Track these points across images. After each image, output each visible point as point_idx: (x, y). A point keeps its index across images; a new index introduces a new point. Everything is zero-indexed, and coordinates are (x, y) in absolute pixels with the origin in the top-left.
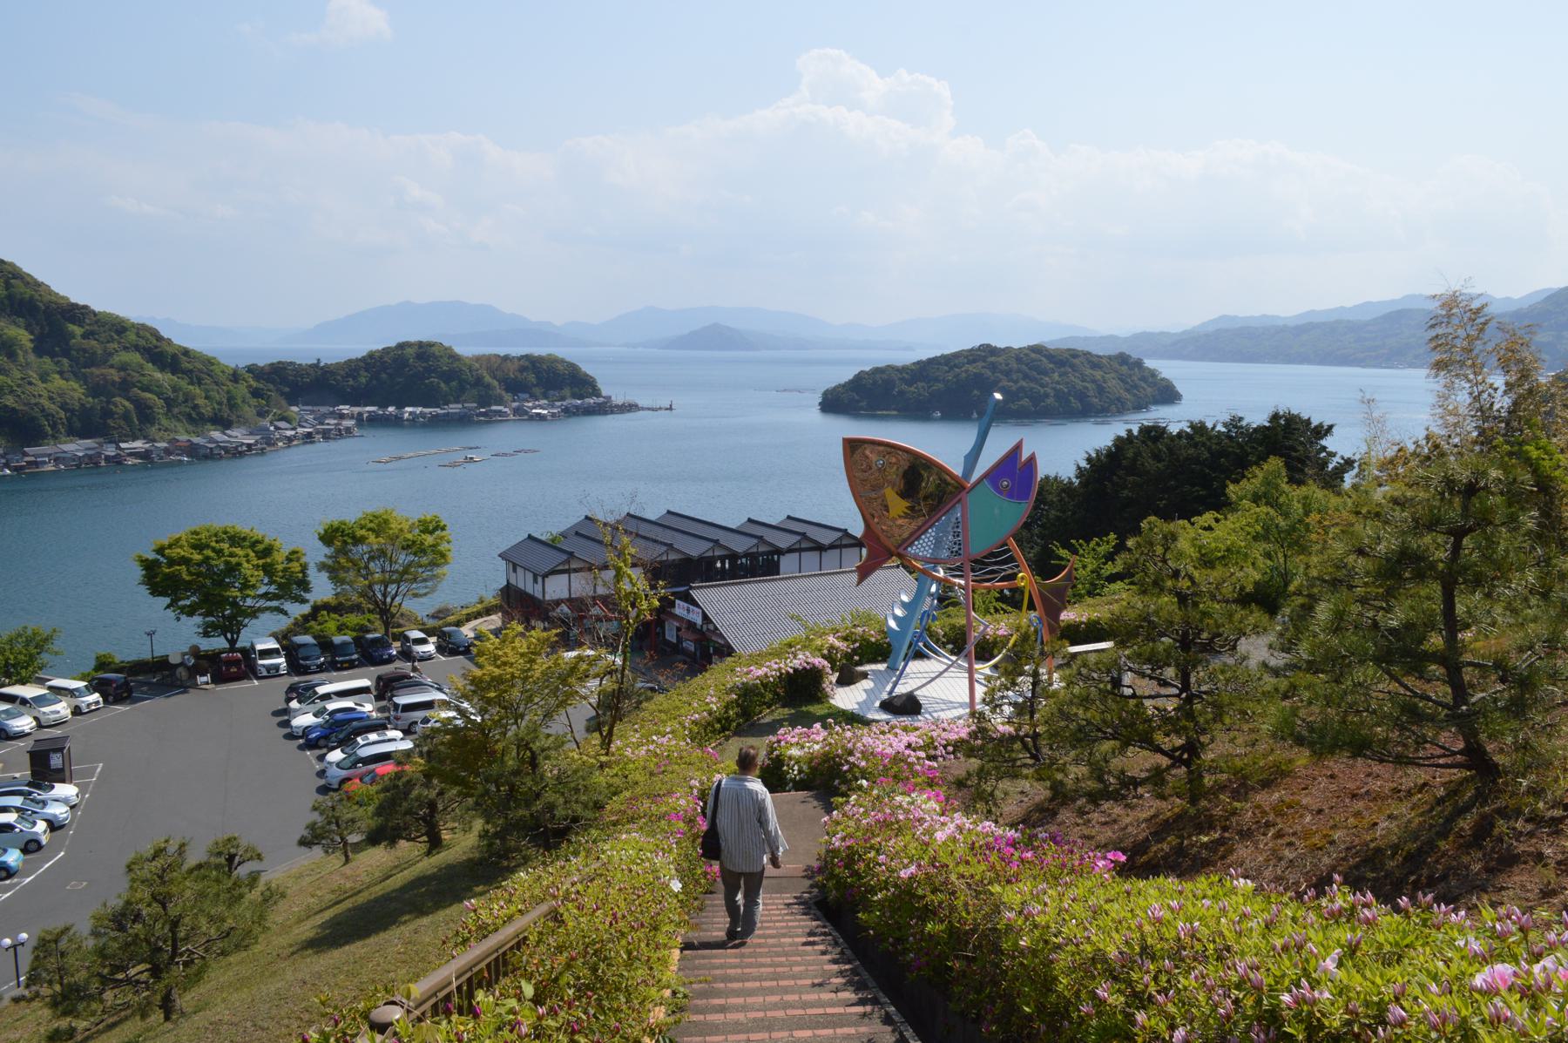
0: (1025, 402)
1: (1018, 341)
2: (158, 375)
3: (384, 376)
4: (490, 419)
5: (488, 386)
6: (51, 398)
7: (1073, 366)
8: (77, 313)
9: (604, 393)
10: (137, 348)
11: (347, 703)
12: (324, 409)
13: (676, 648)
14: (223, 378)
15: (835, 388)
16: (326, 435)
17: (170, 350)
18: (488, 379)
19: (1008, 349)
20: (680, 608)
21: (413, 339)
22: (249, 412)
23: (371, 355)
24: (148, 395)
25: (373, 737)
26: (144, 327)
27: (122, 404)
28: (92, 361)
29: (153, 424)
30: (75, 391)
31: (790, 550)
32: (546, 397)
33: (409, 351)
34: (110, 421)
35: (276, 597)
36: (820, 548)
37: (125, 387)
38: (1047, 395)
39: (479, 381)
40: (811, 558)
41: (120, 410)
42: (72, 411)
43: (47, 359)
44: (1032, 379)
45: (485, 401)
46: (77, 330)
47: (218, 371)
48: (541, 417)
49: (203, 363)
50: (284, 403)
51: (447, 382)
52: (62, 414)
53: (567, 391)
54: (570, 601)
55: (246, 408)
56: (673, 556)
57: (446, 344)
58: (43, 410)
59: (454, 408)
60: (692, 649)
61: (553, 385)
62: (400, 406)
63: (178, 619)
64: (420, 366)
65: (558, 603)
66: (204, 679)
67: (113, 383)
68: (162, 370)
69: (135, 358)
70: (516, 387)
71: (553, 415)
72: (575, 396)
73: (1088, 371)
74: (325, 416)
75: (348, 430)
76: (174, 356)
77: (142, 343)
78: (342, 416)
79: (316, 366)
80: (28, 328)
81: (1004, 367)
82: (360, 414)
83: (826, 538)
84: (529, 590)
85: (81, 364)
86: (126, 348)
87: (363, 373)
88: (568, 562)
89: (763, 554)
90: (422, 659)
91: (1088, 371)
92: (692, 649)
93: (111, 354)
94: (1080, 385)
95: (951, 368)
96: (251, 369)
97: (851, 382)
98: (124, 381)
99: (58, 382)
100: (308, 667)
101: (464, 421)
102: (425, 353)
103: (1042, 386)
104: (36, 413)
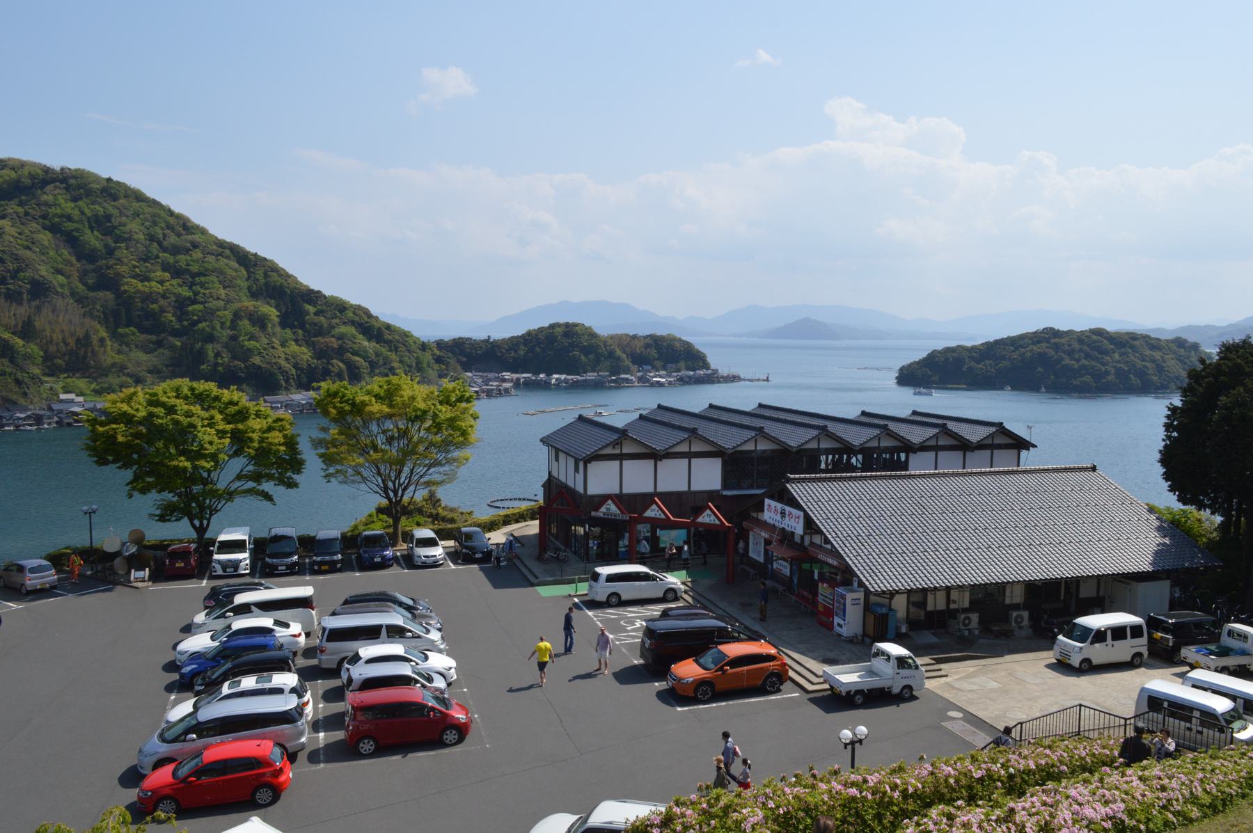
0: (1087, 378)
1: (1080, 326)
2: (366, 343)
3: (538, 349)
4: (619, 385)
5: (619, 359)
6: (287, 359)
7: (1132, 347)
8: (312, 296)
9: (712, 367)
10: (353, 323)
11: (266, 621)
12: (491, 375)
13: (764, 570)
14: (414, 347)
15: (910, 365)
16: (489, 394)
17: (377, 325)
18: (619, 352)
19: (1070, 332)
20: (772, 512)
21: (562, 320)
22: (432, 374)
23: (529, 333)
24: (357, 358)
25: (249, 682)
26: (359, 307)
28: (320, 332)
30: (304, 354)
31: (923, 448)
32: (664, 368)
33: (559, 329)
35: (257, 477)
36: (964, 446)
37: (340, 352)
38: (1107, 373)
39: (611, 354)
40: (950, 462)
41: (336, 370)
42: (302, 369)
43: (288, 331)
44: (1096, 359)
45: (615, 370)
47: (411, 342)
48: (660, 384)
49: (400, 335)
50: (459, 368)
51: (586, 355)
52: (294, 371)
53: (682, 364)
54: (620, 499)
55: (431, 371)
56: (763, 446)
57: (587, 325)
58: (280, 368)
59: (591, 376)
60: (787, 571)
61: (673, 356)
62: (549, 374)
63: (130, 496)
64: (566, 342)
65: (604, 499)
66: (141, 574)
67: (333, 349)
68: (369, 340)
69: (350, 330)
70: (640, 360)
71: (670, 383)
72: (688, 369)
73: (1148, 352)
74: (490, 380)
75: (506, 390)
77: (357, 319)
78: (504, 380)
79: (487, 341)
80: (277, 307)
81: (1066, 347)
82: (518, 379)
83: (974, 435)
84: (570, 483)
85: (310, 333)
86: (345, 323)
87: (522, 347)
88: (615, 444)
89: (886, 450)
90: (425, 566)
91: (1148, 352)
92: (787, 571)
93: (333, 327)
94: (1139, 364)
95: (1016, 349)
96: (440, 344)
97: (925, 359)
98: (341, 347)
99: (294, 347)
100: (275, 567)
101: (598, 386)
102: (571, 332)
103: (1103, 364)
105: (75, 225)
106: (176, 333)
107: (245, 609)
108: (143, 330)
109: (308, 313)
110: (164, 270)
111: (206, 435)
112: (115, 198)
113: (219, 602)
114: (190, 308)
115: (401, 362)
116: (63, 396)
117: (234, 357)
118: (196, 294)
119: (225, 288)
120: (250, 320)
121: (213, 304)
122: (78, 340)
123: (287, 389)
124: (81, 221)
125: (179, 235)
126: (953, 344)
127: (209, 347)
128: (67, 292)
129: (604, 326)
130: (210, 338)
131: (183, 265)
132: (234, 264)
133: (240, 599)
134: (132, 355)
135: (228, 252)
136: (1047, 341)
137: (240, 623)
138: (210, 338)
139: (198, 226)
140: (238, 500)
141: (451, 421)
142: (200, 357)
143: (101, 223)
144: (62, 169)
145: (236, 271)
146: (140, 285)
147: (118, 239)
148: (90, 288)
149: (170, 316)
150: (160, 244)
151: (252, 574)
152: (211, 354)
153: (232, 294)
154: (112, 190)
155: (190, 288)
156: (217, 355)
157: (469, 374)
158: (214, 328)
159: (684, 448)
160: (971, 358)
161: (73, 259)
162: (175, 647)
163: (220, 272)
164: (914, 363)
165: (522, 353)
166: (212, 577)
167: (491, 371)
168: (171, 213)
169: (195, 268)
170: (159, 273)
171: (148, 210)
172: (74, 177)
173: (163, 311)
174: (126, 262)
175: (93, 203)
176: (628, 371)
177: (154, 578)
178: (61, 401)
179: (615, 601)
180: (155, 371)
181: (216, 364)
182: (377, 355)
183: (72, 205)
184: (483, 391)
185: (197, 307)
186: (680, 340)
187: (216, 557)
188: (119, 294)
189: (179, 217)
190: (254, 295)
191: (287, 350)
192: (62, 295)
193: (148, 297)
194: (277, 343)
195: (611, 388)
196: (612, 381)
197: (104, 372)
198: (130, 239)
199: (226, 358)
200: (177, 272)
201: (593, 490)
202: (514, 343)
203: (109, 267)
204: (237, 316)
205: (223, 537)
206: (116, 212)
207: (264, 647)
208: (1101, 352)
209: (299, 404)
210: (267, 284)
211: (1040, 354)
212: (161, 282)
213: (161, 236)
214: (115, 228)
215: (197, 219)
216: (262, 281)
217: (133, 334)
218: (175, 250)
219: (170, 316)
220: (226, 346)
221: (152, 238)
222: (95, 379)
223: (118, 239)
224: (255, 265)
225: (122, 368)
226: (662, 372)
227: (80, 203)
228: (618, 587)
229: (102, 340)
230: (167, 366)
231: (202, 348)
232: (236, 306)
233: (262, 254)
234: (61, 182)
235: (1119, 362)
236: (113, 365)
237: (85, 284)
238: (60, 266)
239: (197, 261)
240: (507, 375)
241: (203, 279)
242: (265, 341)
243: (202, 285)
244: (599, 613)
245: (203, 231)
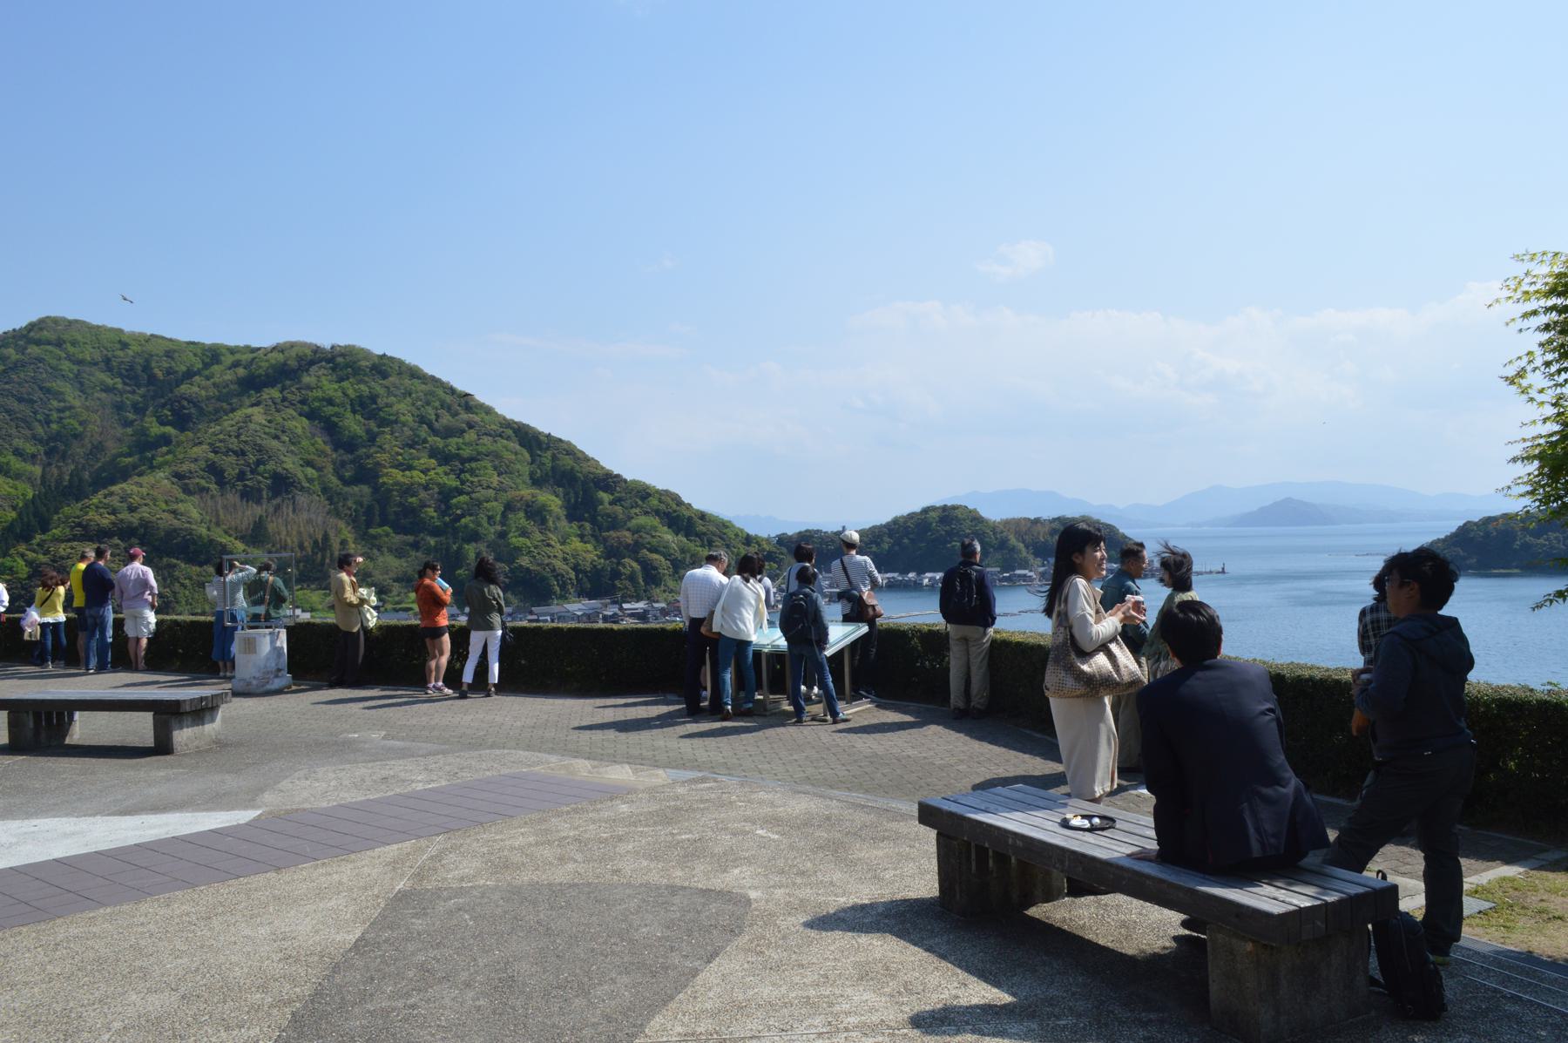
5: (1013, 549)
6: (565, 559)
8: (609, 481)
10: (657, 512)
18: (1013, 541)
23: (895, 521)
24: (655, 556)
26: (667, 492)
27: (630, 565)
28: (615, 524)
29: (658, 585)
30: (589, 553)
33: (932, 514)
34: (617, 583)
37: (634, 549)
39: (1003, 544)
42: (585, 572)
46: (605, 497)
49: (717, 526)
52: (572, 575)
58: (554, 570)
62: (921, 572)
64: (942, 530)
76: (690, 518)
77: (662, 507)
86: (646, 513)
87: (886, 539)
98: (636, 543)
99: (576, 544)
104: (547, 573)
105: (336, 409)
106: (435, 532)
108: (399, 529)
110: (431, 457)
121: (481, 494)
124: (342, 405)
128: (317, 487)
130: (474, 537)
135: (510, 432)
143: (366, 406)
147: (383, 423)
149: (431, 512)
150: (430, 426)
158: (479, 524)
161: (328, 449)
163: (497, 456)
165: (886, 546)
168: (452, 391)
169: (466, 453)
172: (343, 355)
176: (1025, 565)
182: (683, 551)
185: (463, 498)
190: (536, 482)
191: (567, 548)
193: (408, 490)
196: (1005, 579)
200: (444, 458)
203: (368, 457)
204: (509, 507)
212: (425, 472)
214: (380, 409)
215: (482, 396)
217: (387, 535)
218: (448, 433)
221: (422, 420)
223: (383, 423)
227: (345, 384)
231: (460, 548)
232: (511, 494)
233: (556, 434)
234: (329, 361)
237: (341, 478)
239: (469, 444)
241: (474, 465)
245: (489, 411)
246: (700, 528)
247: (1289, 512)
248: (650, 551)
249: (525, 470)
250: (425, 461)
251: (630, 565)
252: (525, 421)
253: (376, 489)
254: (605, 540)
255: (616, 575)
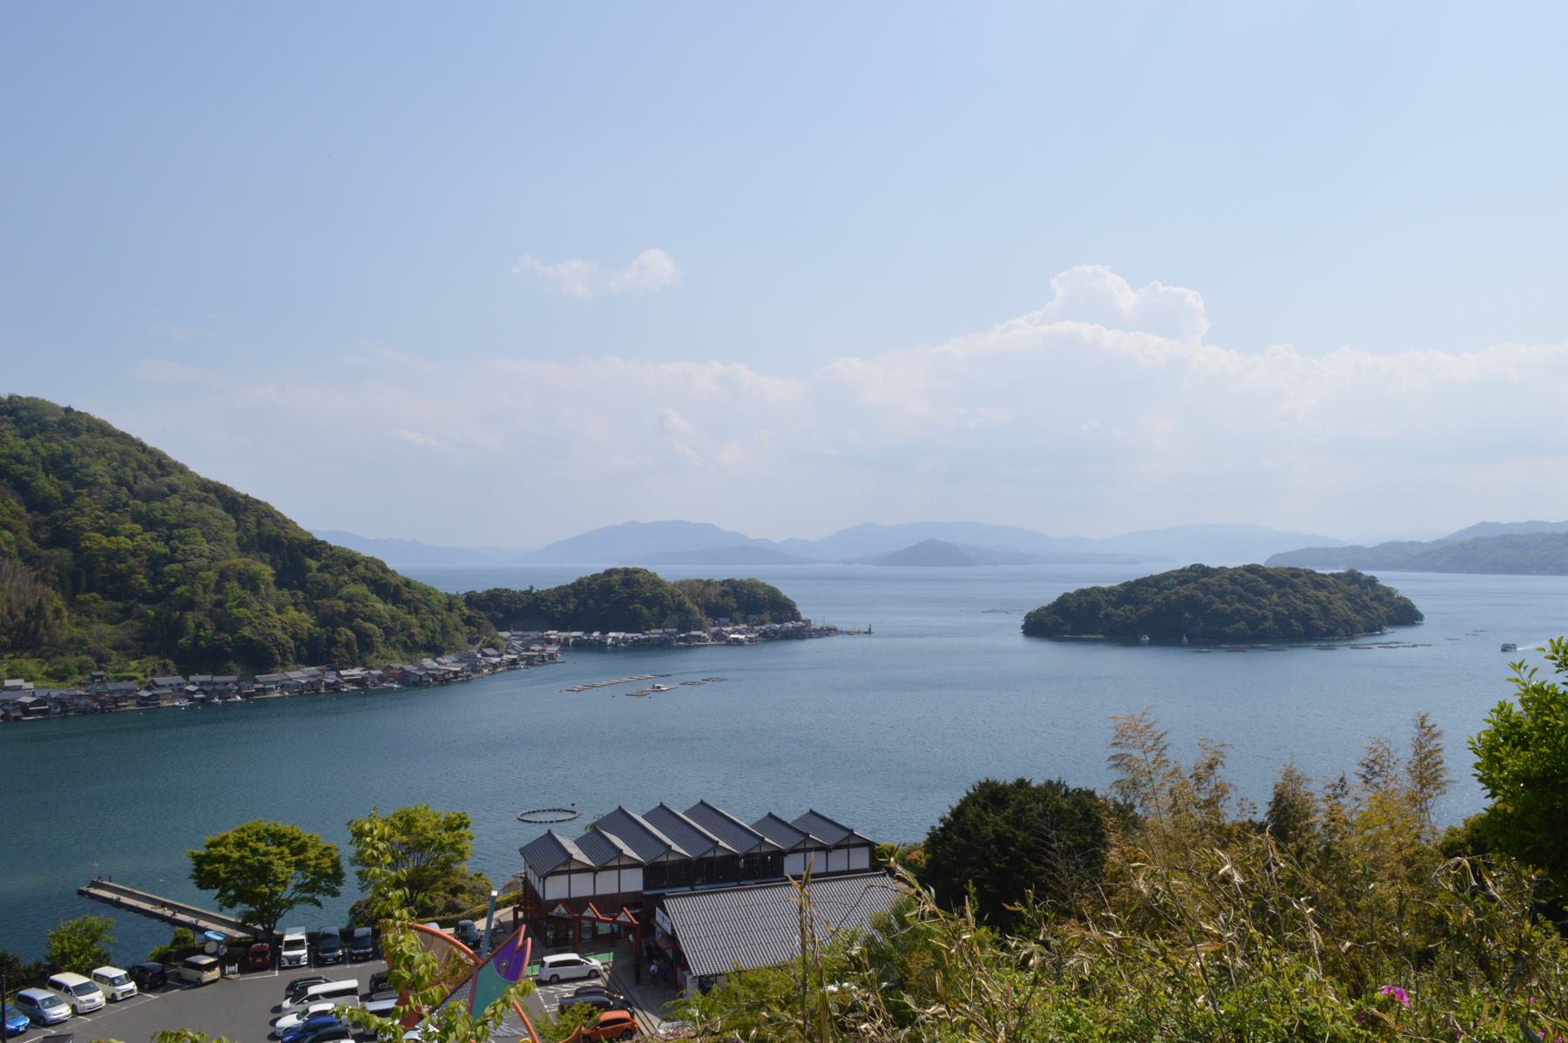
0: (1242, 625)
1: (1232, 563)
2: (380, 606)
4: (690, 644)
5: (689, 612)
6: (284, 629)
7: (1293, 587)
8: (314, 548)
9: (804, 616)
10: (364, 580)
12: (533, 634)
14: (438, 608)
16: (530, 662)
18: (689, 604)
19: (1222, 569)
23: (580, 582)
24: (369, 625)
26: (372, 560)
27: (346, 633)
30: (305, 621)
32: (745, 621)
33: (615, 577)
37: (349, 617)
38: (1265, 618)
39: (680, 607)
42: (302, 640)
43: (285, 592)
45: (685, 625)
46: (313, 563)
48: (738, 642)
51: (649, 608)
52: (292, 644)
53: (766, 616)
59: (655, 633)
62: (604, 632)
65: (556, 902)
66: (232, 968)
67: (340, 614)
68: (385, 602)
69: (361, 589)
70: (716, 612)
71: (751, 640)
72: (774, 621)
73: (1312, 592)
75: (551, 656)
76: (397, 587)
77: (369, 574)
78: (549, 642)
80: (272, 563)
82: (566, 639)
87: (572, 599)
88: (565, 864)
91: (1312, 592)
94: (1302, 606)
95: (1160, 590)
96: (471, 599)
98: (349, 611)
99: (292, 613)
100: (326, 959)
101: (663, 646)
103: (1260, 608)
104: (269, 643)
105: (26, 468)
106: (149, 600)
107: (315, 998)
108: (107, 595)
109: (309, 569)
110: (135, 521)
111: (279, 867)
112: (76, 433)
113: (297, 992)
114: (166, 569)
115: (422, 626)
116: (8, 683)
117: (219, 629)
118: (174, 550)
119: (209, 541)
120: (239, 580)
121: (194, 562)
122: (28, 612)
123: (283, 665)
124: (32, 463)
125: (153, 476)
126: (1087, 586)
127: (189, 615)
128: (14, 551)
129: (670, 572)
130: (190, 605)
131: (158, 514)
132: (219, 511)
133: (312, 990)
134: (95, 628)
135: (212, 496)
136: (1195, 580)
137: (315, 1008)
138: (190, 605)
139: (175, 463)
140: (297, 907)
141: (452, 844)
142: (177, 628)
143: (58, 465)
144: (11, 398)
145: (222, 519)
146: (104, 541)
147: (79, 484)
148: (43, 545)
149: (141, 579)
150: (130, 488)
151: (309, 965)
152: (191, 624)
153: (218, 549)
154: (72, 423)
155: (167, 543)
156: (199, 626)
157: (506, 634)
158: (195, 593)
159: (615, 863)
160: (1108, 602)
161: (22, 509)
162: (273, 1023)
163: (204, 522)
164: (1043, 608)
165: (571, 606)
166: (281, 969)
167: (533, 629)
168: (143, 448)
169: (172, 518)
170: (128, 526)
171: (116, 446)
172: (26, 408)
173: (132, 571)
174: (87, 512)
175: (49, 440)
176: (699, 626)
177: (242, 971)
178: (7, 689)
179: (556, 980)
180: (120, 647)
181: (198, 637)
182: (394, 619)
183: (22, 442)
184: (522, 659)
185: (176, 567)
186: (764, 585)
187: (284, 953)
188: (78, 552)
189: (152, 453)
190: (244, 549)
191: (284, 617)
192: (9, 555)
193: (114, 556)
194: (271, 608)
195: (679, 647)
196: (682, 639)
197: (60, 650)
198: (93, 483)
199: (209, 630)
200: (150, 524)
201: (549, 897)
202: (562, 594)
203: (66, 519)
204: (223, 576)
205: (287, 938)
206: (77, 451)
207: (331, 1024)
208: (1256, 594)
209: (298, 685)
210: (260, 535)
211: (1187, 597)
212: (131, 536)
213: (131, 479)
214: (75, 470)
215: (175, 453)
216: (254, 531)
217: (95, 601)
218: (149, 496)
219: (141, 579)
220: (210, 614)
221: (120, 482)
222: (47, 659)
223: (79, 484)
224: (246, 509)
225: (79, 645)
226: (743, 626)
227: (32, 440)
228: (558, 970)
229: (57, 612)
230: (137, 640)
231: (181, 618)
232: (222, 564)
233: (254, 494)
234: (10, 413)
235: (1277, 605)
236: (71, 640)
237: (36, 540)
238: (7, 519)
239: (175, 509)
240: (553, 634)
241: (182, 531)
242: (257, 607)
243: (181, 539)
244: (543, 989)
245: (182, 469)
246: (406, 596)
247: (932, 553)
248: (365, 620)
249: (231, 535)
250: (129, 526)
251: (346, 633)
252: (223, 482)
253: (78, 552)
254: (316, 608)
255: (332, 642)
